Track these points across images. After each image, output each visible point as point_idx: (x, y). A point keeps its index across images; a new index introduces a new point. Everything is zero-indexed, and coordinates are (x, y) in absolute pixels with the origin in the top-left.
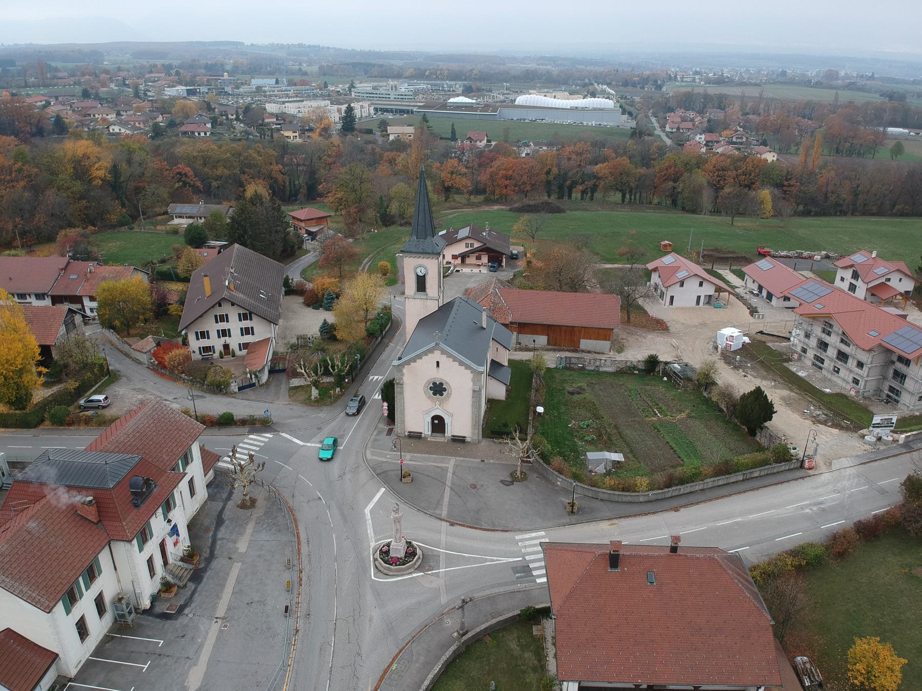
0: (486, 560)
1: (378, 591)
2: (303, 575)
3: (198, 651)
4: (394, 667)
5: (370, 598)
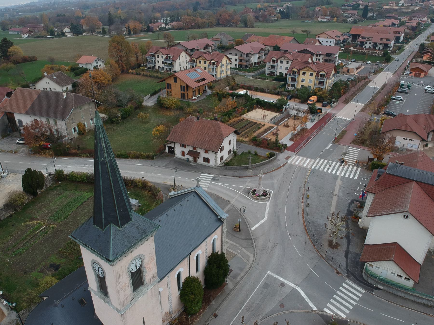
0: (225, 185)
1: (272, 187)
2: (301, 201)
3: (340, 189)
5: (276, 186)
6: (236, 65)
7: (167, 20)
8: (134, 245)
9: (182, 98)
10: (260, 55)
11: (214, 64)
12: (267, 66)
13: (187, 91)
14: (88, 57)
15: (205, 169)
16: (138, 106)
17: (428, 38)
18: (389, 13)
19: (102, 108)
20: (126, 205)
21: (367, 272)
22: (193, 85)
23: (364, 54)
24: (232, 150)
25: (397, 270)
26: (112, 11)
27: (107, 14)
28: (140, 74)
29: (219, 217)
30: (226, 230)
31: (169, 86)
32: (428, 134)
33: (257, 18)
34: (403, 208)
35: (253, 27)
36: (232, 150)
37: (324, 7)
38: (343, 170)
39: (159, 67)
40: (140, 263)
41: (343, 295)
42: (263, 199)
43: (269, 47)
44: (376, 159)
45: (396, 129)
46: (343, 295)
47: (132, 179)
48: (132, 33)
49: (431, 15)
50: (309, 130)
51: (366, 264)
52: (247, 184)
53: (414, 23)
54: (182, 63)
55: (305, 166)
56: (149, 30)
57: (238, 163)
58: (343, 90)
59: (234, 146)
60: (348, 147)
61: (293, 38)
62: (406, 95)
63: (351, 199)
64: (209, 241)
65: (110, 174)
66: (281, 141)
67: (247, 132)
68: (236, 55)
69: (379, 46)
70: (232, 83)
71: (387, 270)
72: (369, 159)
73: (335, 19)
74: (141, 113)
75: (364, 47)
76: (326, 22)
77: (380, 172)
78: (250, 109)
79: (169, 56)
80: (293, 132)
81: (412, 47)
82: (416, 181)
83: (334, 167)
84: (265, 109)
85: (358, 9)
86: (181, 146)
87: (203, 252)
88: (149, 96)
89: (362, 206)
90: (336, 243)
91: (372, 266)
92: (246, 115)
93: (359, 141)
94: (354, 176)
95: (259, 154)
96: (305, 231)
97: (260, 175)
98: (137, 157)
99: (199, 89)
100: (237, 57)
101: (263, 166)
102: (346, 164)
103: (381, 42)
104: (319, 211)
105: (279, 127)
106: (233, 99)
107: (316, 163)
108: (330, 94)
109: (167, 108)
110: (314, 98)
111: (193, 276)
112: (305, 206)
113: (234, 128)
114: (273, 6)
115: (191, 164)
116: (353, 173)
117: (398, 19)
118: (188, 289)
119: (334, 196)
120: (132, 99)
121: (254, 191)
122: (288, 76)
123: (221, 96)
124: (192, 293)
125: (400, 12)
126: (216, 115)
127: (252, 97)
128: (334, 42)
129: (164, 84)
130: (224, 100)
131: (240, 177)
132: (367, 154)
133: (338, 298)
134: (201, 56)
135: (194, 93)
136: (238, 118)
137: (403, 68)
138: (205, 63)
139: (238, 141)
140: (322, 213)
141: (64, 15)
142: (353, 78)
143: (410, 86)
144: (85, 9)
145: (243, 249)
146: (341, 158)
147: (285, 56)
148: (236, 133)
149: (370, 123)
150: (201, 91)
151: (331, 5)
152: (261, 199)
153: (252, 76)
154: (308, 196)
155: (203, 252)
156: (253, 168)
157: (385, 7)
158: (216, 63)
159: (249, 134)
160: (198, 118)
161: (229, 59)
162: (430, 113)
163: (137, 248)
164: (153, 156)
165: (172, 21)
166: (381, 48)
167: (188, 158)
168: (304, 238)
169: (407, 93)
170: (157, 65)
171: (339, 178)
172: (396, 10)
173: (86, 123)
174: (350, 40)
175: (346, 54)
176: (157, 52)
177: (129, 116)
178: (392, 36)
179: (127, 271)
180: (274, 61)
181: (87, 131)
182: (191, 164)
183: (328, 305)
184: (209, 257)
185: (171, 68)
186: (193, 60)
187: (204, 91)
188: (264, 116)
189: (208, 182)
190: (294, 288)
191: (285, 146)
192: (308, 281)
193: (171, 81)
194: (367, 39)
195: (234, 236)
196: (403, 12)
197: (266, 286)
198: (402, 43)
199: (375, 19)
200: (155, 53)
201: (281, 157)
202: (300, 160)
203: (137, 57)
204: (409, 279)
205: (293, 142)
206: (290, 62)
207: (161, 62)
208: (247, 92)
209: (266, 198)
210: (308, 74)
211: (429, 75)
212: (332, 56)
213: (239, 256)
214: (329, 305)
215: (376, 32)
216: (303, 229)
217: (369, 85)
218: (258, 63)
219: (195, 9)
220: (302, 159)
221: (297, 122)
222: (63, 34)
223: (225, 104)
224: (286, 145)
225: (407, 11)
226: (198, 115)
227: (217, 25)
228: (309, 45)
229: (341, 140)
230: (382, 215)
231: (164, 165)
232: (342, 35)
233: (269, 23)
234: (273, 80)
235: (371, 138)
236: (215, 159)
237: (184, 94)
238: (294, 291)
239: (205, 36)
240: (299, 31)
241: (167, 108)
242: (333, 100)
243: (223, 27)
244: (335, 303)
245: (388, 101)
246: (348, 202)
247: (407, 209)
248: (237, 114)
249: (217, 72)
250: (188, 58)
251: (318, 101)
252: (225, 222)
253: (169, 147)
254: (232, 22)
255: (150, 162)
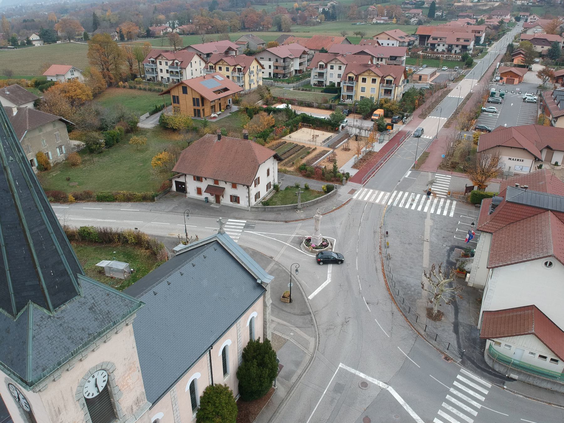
0: (265, 235)
1: (334, 234)
4: (334, 208)
5: (339, 232)
6: (270, 74)
7: (174, 24)
8: (86, 344)
9: (195, 116)
10: (302, 60)
11: (239, 70)
12: (313, 74)
13: (203, 105)
14: (60, 66)
16: (132, 128)
17: (515, 38)
18: (462, 11)
19: (76, 133)
20: (62, 263)
21: (492, 355)
22: (211, 97)
23: (438, 58)
25: (539, 348)
26: (99, 13)
27: (92, 18)
28: (135, 88)
29: (259, 281)
30: (271, 301)
31: (176, 100)
32: (541, 151)
33: (294, 20)
34: (544, 251)
35: (289, 31)
37: (379, 5)
39: (162, 78)
40: (106, 378)
41: (460, 395)
44: (476, 188)
45: (499, 146)
46: (460, 395)
47: (119, 231)
48: (126, 39)
49: (515, 13)
50: (378, 153)
51: (488, 342)
52: (296, 231)
53: (495, 21)
54: (194, 71)
55: (377, 201)
56: (149, 34)
57: (281, 203)
58: (417, 101)
59: (274, 178)
60: (434, 173)
61: (344, 38)
62: (499, 105)
64: (244, 323)
65: (16, 195)
66: (341, 169)
67: (291, 159)
68: (270, 60)
69: (455, 49)
70: (267, 95)
71: (522, 348)
72: (466, 187)
73: (394, 21)
74: (135, 137)
75: (435, 50)
76: (383, 24)
77: (495, 201)
78: (294, 128)
79: (176, 61)
80: (357, 156)
81: (498, 48)
82: (552, 211)
84: (314, 129)
85: (423, 8)
86: (194, 180)
87: (234, 342)
89: (469, 254)
90: (438, 311)
91: (500, 344)
92: (288, 136)
93: (450, 165)
94: (449, 213)
96: (390, 297)
97: (317, 215)
98: (128, 199)
99: (220, 104)
100: (271, 63)
102: (436, 197)
103: (458, 43)
104: (407, 264)
105: (335, 151)
108: (400, 107)
109: (174, 130)
110: (380, 112)
111: (217, 383)
112: (384, 259)
114: (314, 5)
115: (212, 206)
116: (449, 209)
117: (474, 19)
118: (210, 408)
120: (121, 118)
121: (309, 240)
122: (341, 86)
123: (251, 112)
124: (217, 413)
125: (476, 10)
127: (295, 112)
128: (396, 44)
130: (255, 117)
131: (286, 222)
132: (464, 181)
133: (453, 400)
136: (277, 141)
137: (491, 70)
138: (228, 70)
139: (279, 171)
140: (411, 268)
141: (33, 20)
143: (503, 95)
144: (62, 14)
145: (298, 330)
146: (427, 188)
147: (336, 59)
148: (276, 157)
149: (460, 142)
151: (388, 4)
153: (294, 87)
154: (388, 243)
155: (233, 342)
156: (304, 207)
157: (456, 4)
159: (294, 162)
163: (93, 351)
164: (153, 197)
165: (181, 24)
166: (458, 51)
167: (207, 198)
168: (389, 306)
169: (501, 103)
170: (160, 75)
171: (429, 216)
172: (470, 8)
173: (50, 153)
174: (417, 43)
175: (414, 58)
176: (159, 56)
177: (117, 142)
178: (472, 36)
179: (76, 399)
180: (321, 67)
181: (52, 165)
182: (212, 206)
183: (439, 413)
184: (245, 349)
189: (238, 231)
190: (382, 389)
191: (347, 176)
192: (404, 375)
193: (177, 92)
194: (439, 40)
195: (283, 310)
196: (480, 10)
197: (338, 388)
198: (484, 44)
199: (445, 20)
200: (156, 59)
201: (343, 191)
204: (557, 361)
205: (358, 171)
206: (343, 67)
207: (164, 71)
210: (369, 80)
212: (398, 59)
213: (292, 344)
214: (440, 412)
215: (451, 32)
216: (387, 293)
217: (449, 95)
218: (300, 71)
219: (211, 9)
222: (29, 43)
224: (348, 174)
225: (485, 8)
227: (242, 29)
228: (366, 46)
229: (423, 165)
231: (171, 208)
232: (407, 36)
233: (311, 26)
234: (322, 92)
235: (462, 160)
237: (199, 111)
238: (384, 394)
241: (174, 130)
242: (406, 114)
244: (450, 408)
245: (477, 113)
246: (446, 250)
247: (551, 252)
249: (244, 82)
250: (203, 65)
251: (386, 116)
252: (268, 288)
254: (261, 25)
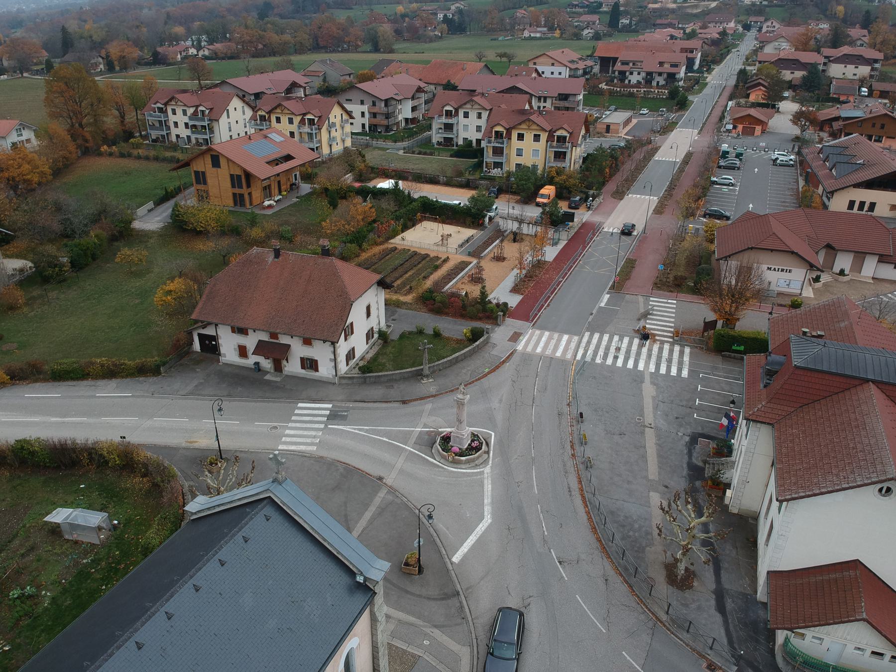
0: (367, 431)
1: (490, 422)
2: (570, 452)
3: (656, 408)
4: (487, 370)
5: (499, 417)
6: (363, 125)
7: (199, 41)
9: (235, 204)
10: (416, 103)
11: (311, 122)
12: (435, 126)
13: (249, 186)
15: (307, 387)
17: (747, 59)
18: (661, 16)
22: (262, 171)
23: (631, 95)
24: (376, 330)
26: (73, 26)
28: (129, 155)
29: (360, 579)
31: (201, 178)
33: (398, 32)
35: (392, 51)
36: (376, 330)
37: (532, 9)
38: (649, 356)
39: (178, 136)
42: (473, 460)
43: (432, 87)
45: (752, 248)
48: (117, 68)
49: (742, 18)
50: (551, 263)
52: (424, 420)
53: (713, 32)
54: (233, 124)
56: (158, 60)
57: (396, 364)
59: (379, 319)
61: (484, 64)
62: (736, 172)
63: (689, 431)
67: (407, 279)
68: (362, 103)
73: (557, 33)
74: (126, 251)
75: (627, 82)
76: (540, 39)
78: (409, 223)
79: (201, 108)
81: (722, 76)
82: (874, 382)
83: (628, 352)
84: (443, 222)
86: (233, 331)
88: (150, 205)
91: (803, 636)
92: (399, 237)
93: (670, 283)
95: (445, 334)
98: (111, 373)
99: (279, 182)
100: (365, 108)
101: (459, 365)
102: (655, 341)
103: (661, 70)
106: (365, 201)
107: (583, 344)
108: (582, 180)
109: (199, 233)
112: (581, 467)
113: (376, 271)
115: (268, 377)
116: (677, 362)
117: (679, 28)
119: (647, 429)
121: (446, 439)
123: (335, 196)
126: (325, 242)
127: (409, 194)
128: (566, 73)
129: (187, 175)
130: (343, 205)
131: (404, 402)
132: (700, 311)
134: (279, 105)
135: (267, 191)
138: (291, 121)
139: (388, 303)
142: (622, 144)
143: (741, 154)
144: (13, 28)
145: (437, 633)
147: (473, 101)
148: (383, 284)
150: (282, 184)
151: (546, 6)
152: (468, 462)
153: (404, 149)
157: (651, 6)
158: (316, 120)
159: (413, 284)
160: (277, 254)
161: (350, 114)
162: (797, 207)
165: (211, 42)
166: (662, 82)
167: (257, 364)
168: (598, 566)
169: (739, 169)
170: (174, 132)
171: (647, 379)
172: (673, 11)
174: (596, 69)
176: (170, 100)
178: (682, 58)
180: (449, 114)
182: (268, 377)
185: (207, 137)
186: (261, 116)
187: (292, 185)
188: (445, 238)
189: (316, 426)
193: (204, 165)
194: (631, 64)
195: (407, 592)
198: (698, 71)
199: (636, 31)
200: (166, 104)
201: (499, 335)
202: (544, 339)
203: (122, 117)
206: (485, 115)
207: (181, 125)
208: (397, 183)
209: (478, 458)
210: (529, 136)
211: (771, 130)
212: (571, 99)
215: (650, 51)
216: (591, 538)
217: (657, 157)
218: (413, 120)
219: (262, 15)
220: (550, 339)
221: (525, 246)
223: (351, 216)
224: (505, 304)
225: (695, 11)
226: (276, 243)
227: (314, 48)
228: (519, 77)
229: (628, 283)
230: (822, 494)
231: (190, 388)
232: (580, 59)
234: (451, 156)
236: (332, 361)
237: (242, 196)
239: (290, 66)
240: (491, 55)
242: (591, 192)
243: (327, 52)
245: (704, 188)
246: (683, 442)
248: (379, 237)
249: (320, 141)
250: (249, 113)
251: (559, 196)
252: (379, 589)
253: (201, 336)
254: (345, 43)
255: (149, 383)
